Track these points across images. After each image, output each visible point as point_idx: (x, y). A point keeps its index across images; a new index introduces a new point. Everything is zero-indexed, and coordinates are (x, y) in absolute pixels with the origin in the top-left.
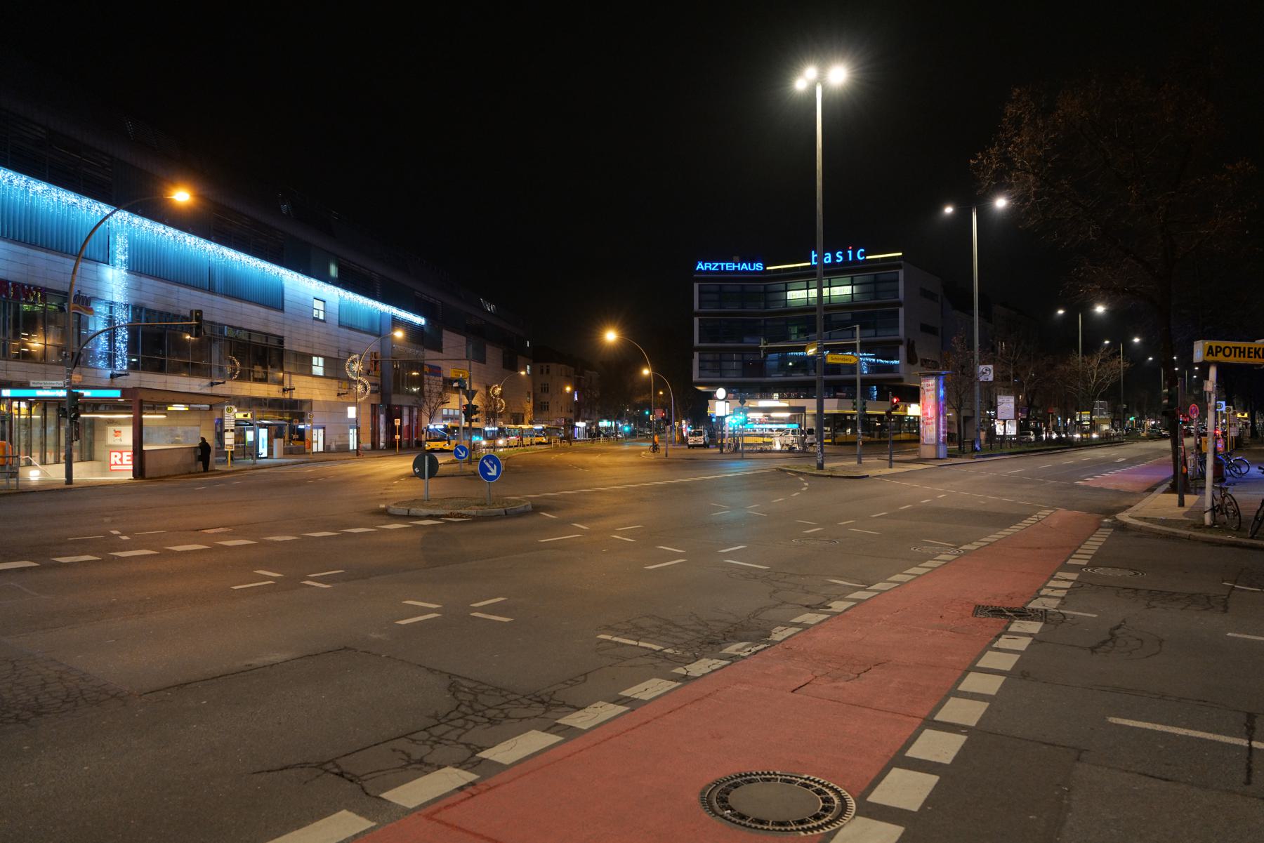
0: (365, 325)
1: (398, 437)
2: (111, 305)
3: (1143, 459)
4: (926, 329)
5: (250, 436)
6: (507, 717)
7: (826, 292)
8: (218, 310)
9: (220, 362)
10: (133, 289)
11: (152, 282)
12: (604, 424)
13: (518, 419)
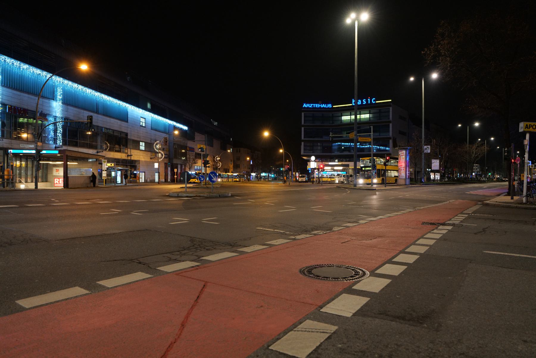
0: (162, 129)
1: (176, 176)
2: (55, 117)
3: (495, 187)
4: (402, 133)
5: (113, 174)
6: (215, 249)
7: (358, 117)
8: (99, 120)
9: (101, 143)
10: (64, 111)
11: (72, 108)
12: (263, 174)
13: (227, 171)
